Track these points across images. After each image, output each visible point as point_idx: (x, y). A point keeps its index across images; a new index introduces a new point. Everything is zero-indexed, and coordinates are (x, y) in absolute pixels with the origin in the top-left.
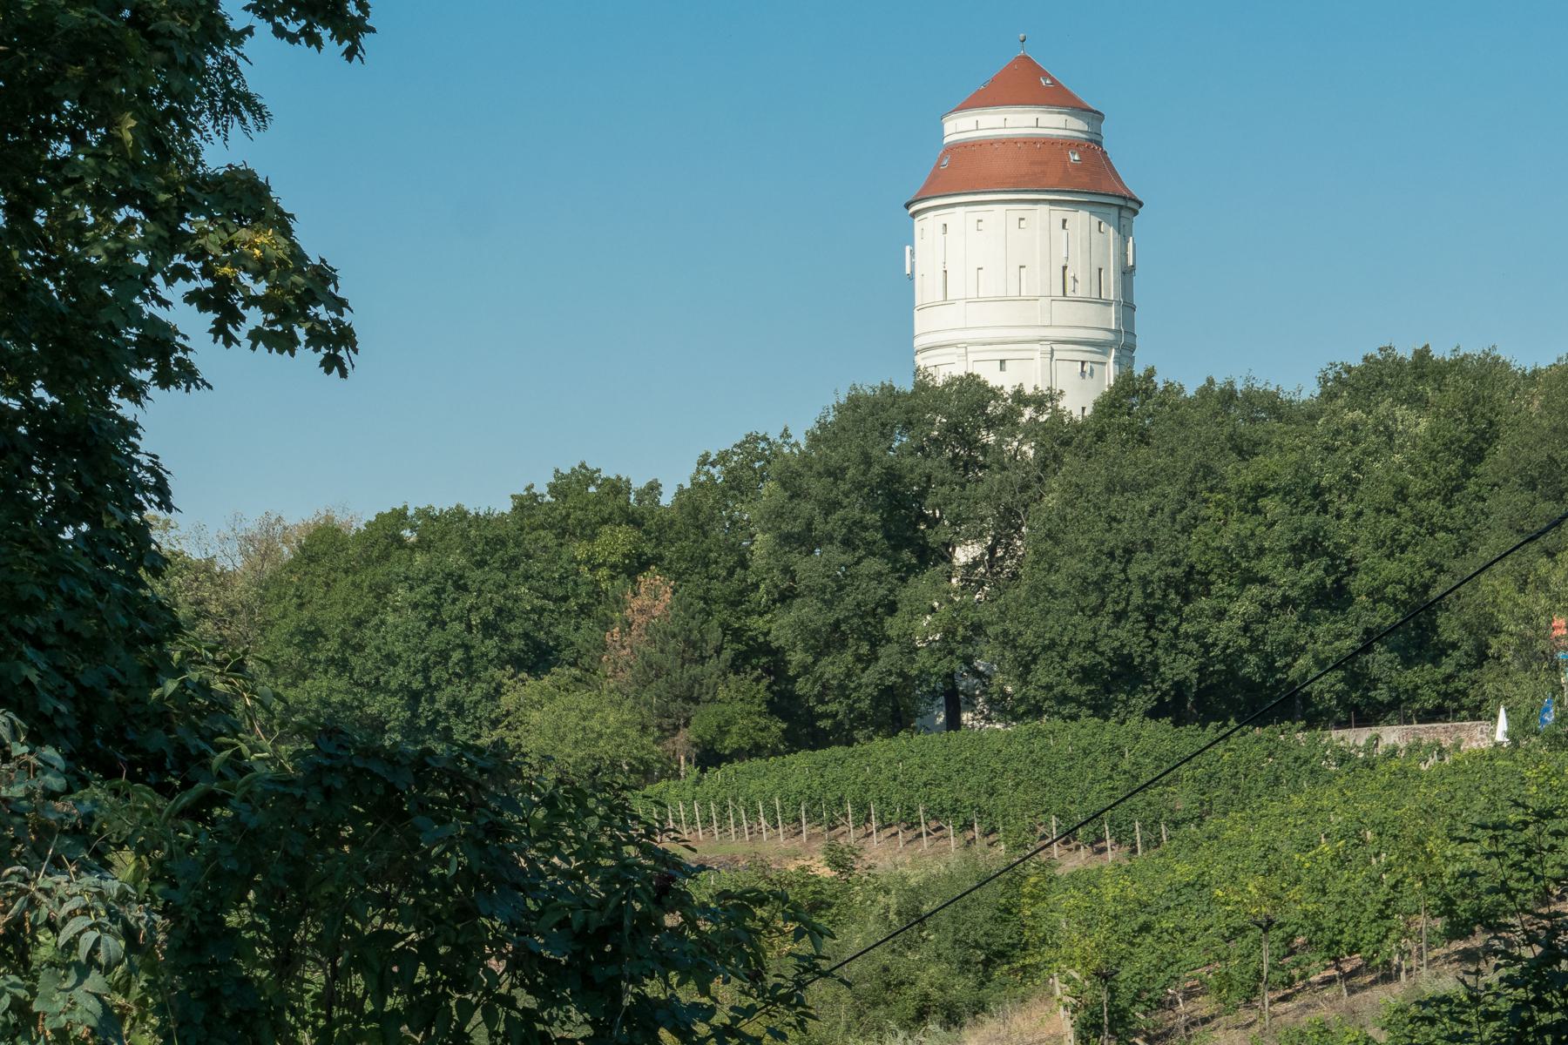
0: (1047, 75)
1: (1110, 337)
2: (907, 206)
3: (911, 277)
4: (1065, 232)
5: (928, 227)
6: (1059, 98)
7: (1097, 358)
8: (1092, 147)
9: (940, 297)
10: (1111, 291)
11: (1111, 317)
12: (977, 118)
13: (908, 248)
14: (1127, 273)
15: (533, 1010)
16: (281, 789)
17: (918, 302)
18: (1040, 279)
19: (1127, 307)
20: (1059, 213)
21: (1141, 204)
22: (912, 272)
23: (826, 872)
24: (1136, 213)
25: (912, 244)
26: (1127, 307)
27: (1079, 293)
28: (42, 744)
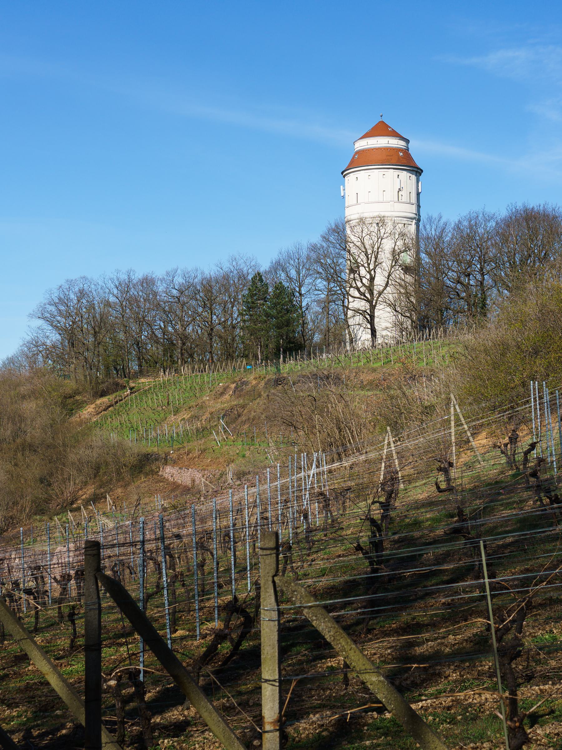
0: (390, 128)
1: (414, 216)
2: (342, 173)
3: (343, 197)
4: (398, 180)
5: (351, 179)
6: (395, 134)
7: (410, 223)
8: (406, 151)
9: (356, 202)
10: (414, 200)
11: (414, 209)
12: (368, 141)
13: (342, 187)
14: (418, 194)
15: (229, 641)
16: (79, 564)
17: (346, 205)
18: (392, 194)
19: (419, 206)
20: (397, 172)
21: (422, 171)
22: (344, 195)
23: (315, 369)
24: (420, 175)
25: (344, 186)
26: (419, 206)
27: (403, 200)
28: (216, 636)
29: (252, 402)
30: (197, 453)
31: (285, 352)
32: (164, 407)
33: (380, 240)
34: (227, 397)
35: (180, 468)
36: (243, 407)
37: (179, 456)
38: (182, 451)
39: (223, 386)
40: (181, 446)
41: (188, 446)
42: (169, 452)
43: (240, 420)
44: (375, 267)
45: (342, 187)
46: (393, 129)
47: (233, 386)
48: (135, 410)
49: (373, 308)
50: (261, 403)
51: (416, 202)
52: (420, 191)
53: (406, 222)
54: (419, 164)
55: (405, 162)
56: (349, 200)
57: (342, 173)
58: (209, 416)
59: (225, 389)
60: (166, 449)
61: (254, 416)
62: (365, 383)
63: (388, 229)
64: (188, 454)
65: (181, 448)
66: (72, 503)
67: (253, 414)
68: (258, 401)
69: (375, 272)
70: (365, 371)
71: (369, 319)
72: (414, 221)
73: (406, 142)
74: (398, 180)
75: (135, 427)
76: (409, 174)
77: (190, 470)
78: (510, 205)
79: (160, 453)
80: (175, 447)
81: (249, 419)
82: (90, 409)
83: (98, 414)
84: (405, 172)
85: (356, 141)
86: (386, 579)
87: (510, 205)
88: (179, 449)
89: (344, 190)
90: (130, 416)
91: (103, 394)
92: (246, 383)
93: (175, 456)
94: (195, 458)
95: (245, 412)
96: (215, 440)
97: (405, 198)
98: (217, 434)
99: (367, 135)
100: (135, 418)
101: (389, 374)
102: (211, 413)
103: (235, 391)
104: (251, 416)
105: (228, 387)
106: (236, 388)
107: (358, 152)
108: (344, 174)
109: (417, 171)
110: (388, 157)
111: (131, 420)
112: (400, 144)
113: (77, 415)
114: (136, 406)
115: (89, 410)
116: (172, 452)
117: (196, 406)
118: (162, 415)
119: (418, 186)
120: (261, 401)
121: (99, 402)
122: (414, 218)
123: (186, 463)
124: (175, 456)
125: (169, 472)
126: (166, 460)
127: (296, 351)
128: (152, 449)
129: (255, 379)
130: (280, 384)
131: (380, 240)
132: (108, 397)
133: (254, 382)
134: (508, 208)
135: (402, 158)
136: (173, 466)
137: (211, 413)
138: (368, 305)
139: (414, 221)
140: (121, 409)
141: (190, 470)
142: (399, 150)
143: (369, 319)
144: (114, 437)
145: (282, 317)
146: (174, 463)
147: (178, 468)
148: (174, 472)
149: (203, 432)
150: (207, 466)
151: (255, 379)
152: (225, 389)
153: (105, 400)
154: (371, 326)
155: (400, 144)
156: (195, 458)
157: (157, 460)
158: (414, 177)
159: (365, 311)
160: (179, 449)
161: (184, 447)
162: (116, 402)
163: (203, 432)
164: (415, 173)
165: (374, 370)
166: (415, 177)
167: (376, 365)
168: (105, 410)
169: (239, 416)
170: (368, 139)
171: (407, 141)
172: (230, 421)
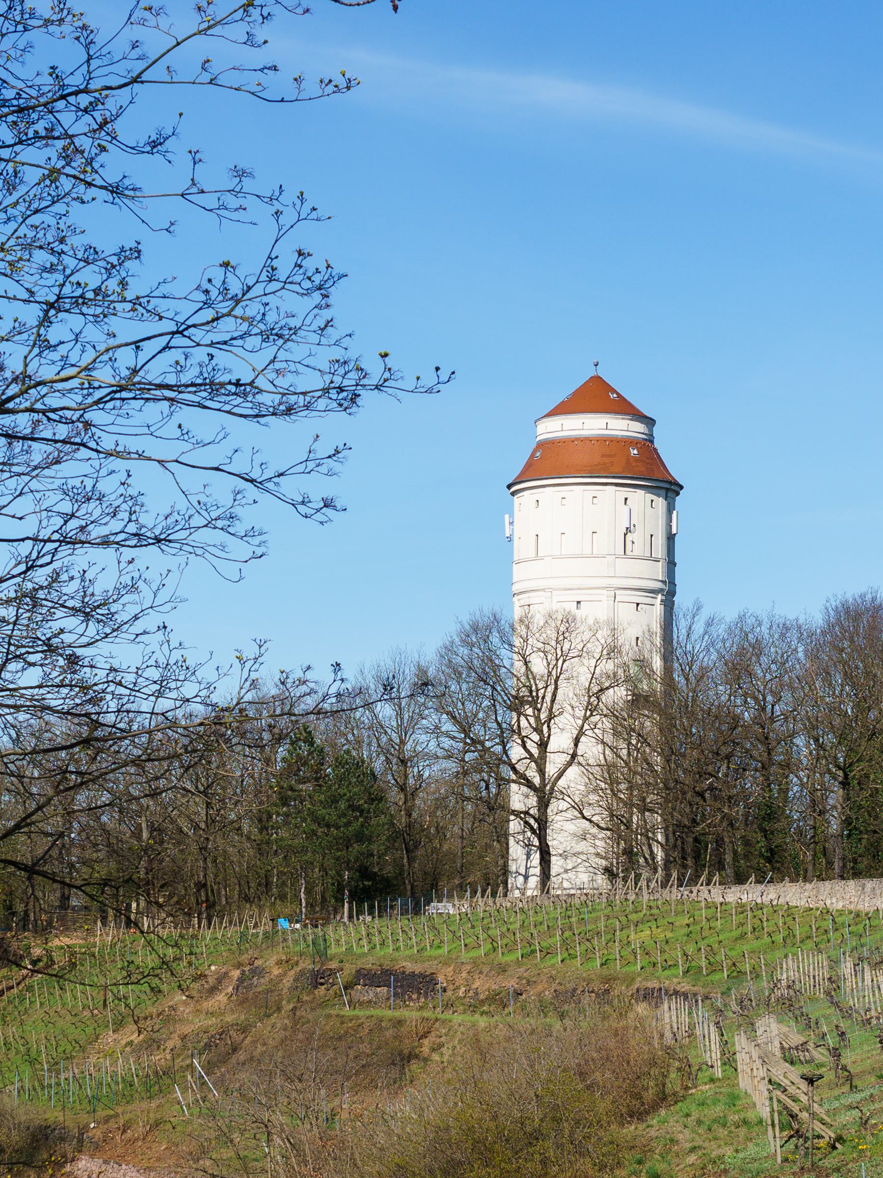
0: (614, 391)
1: (660, 585)
3: (510, 539)
4: (626, 508)
5: (525, 501)
6: (625, 408)
7: (649, 601)
8: (647, 445)
9: (532, 554)
10: (660, 551)
11: (659, 571)
13: (507, 517)
14: (671, 538)
19: (671, 564)
20: (624, 492)
21: (681, 487)
24: (678, 494)
25: (512, 515)
26: (671, 564)
27: (636, 553)
29: (261, 1020)
30: (139, 1130)
31: (352, 897)
32: (96, 1012)
33: (560, 662)
35: (106, 1162)
36: (244, 1029)
37: (105, 1134)
38: (112, 1125)
39: (216, 972)
40: (112, 1112)
42: (88, 1124)
43: (233, 1060)
45: (507, 517)
46: (619, 395)
47: (236, 973)
48: (38, 1013)
50: (279, 1025)
51: (665, 556)
52: (674, 531)
53: (638, 600)
54: (676, 472)
55: (643, 469)
56: (522, 548)
58: (179, 1043)
59: (222, 978)
60: (84, 1118)
61: (263, 1054)
62: (482, 997)
63: (578, 640)
64: (124, 1131)
65: (112, 1116)
67: (260, 1048)
68: (273, 1019)
69: (548, 726)
70: (485, 970)
71: (536, 826)
72: (660, 597)
73: (647, 424)
74: (626, 508)
75: (33, 1054)
76: (650, 496)
77: (124, 1166)
78: (832, 600)
81: (252, 1058)
84: (641, 492)
85: (539, 419)
87: (832, 600)
88: (107, 1120)
89: (511, 523)
92: (257, 972)
93: (98, 1134)
94: (137, 1139)
95: (246, 1042)
96: (179, 1103)
97: (639, 547)
98: (184, 1091)
100: (35, 1034)
101: (528, 982)
102: (183, 1038)
103: (238, 987)
104: (256, 1053)
105: (226, 974)
106: (241, 980)
107: (541, 445)
110: (606, 460)
111: (28, 1037)
114: (42, 1004)
116: (92, 1125)
117: (159, 1015)
118: (89, 1030)
120: (280, 1021)
122: (660, 591)
123: (119, 1150)
124: (98, 1134)
126: (80, 1141)
127: (371, 899)
128: (54, 1115)
129: (279, 963)
130: (322, 984)
131: (560, 662)
133: (276, 971)
134: (828, 604)
135: (636, 460)
136: (92, 1156)
137: (183, 1038)
139: (660, 597)
140: (10, 1008)
141: (124, 1166)
143: (536, 826)
145: (348, 824)
146: (97, 1148)
147: (101, 1161)
148: (94, 1168)
151: (279, 963)
152: (222, 978)
154: (540, 842)
156: (137, 1139)
157: (62, 1139)
158: (660, 503)
159: (527, 813)
161: (117, 1115)
164: (663, 492)
165: (503, 969)
166: (665, 502)
167: (510, 958)
169: (235, 1050)
170: (563, 417)
171: (650, 422)
172: (215, 1059)
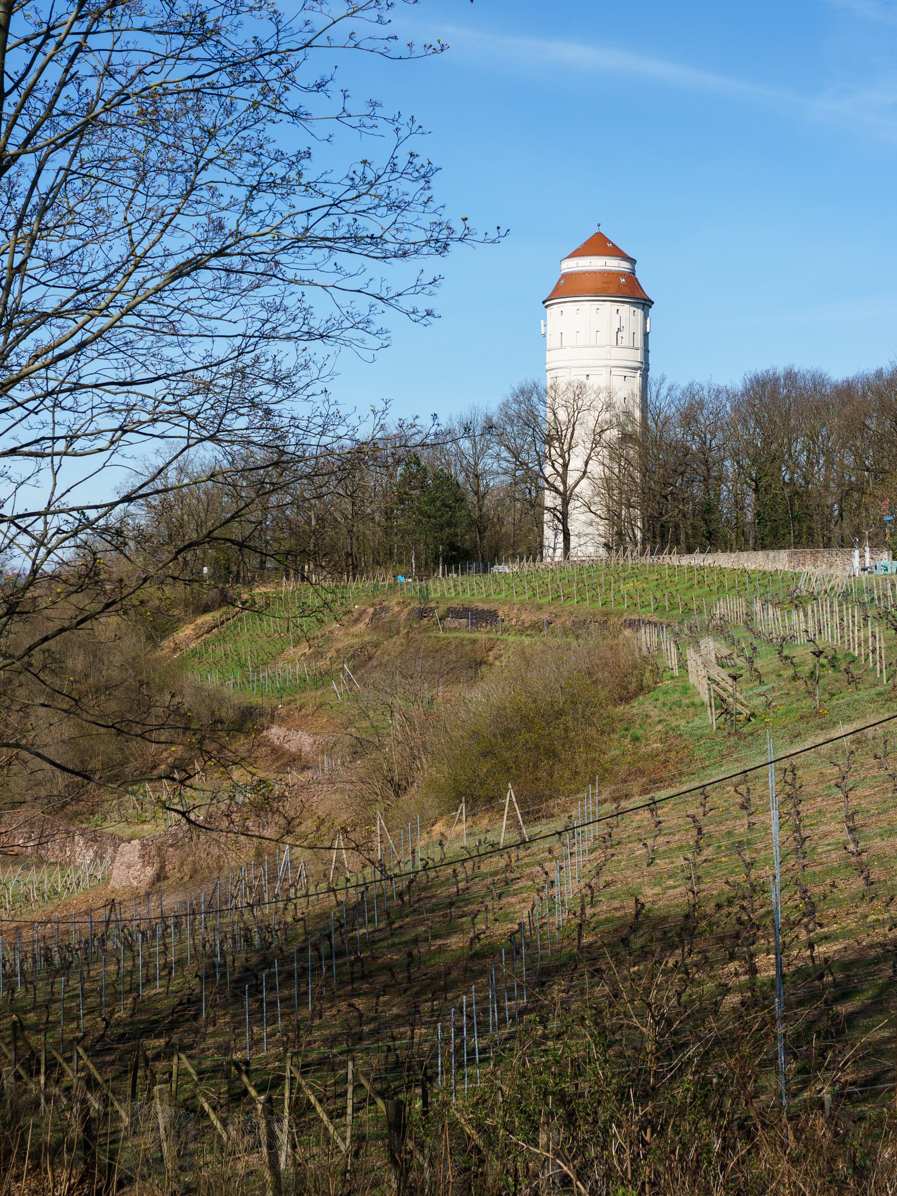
1: (639, 365)
2: (544, 302)
3: (544, 335)
5: (554, 311)
6: (617, 253)
8: (631, 276)
9: (558, 345)
10: (639, 343)
11: (638, 355)
14: (646, 335)
18: (607, 336)
19: (646, 351)
20: (617, 306)
25: (545, 321)
26: (646, 351)
30: (310, 709)
34: (362, 625)
35: (288, 729)
38: (293, 706)
41: (301, 698)
42: (277, 707)
43: (369, 665)
44: (570, 448)
47: (371, 610)
48: (246, 636)
49: (566, 503)
54: (650, 293)
57: (544, 302)
58: (335, 654)
59: (362, 613)
60: (275, 701)
61: (388, 661)
66: (154, 767)
68: (394, 639)
76: (633, 309)
79: (266, 705)
80: (286, 699)
82: (187, 631)
83: (198, 638)
86: (316, 953)
88: (289, 703)
90: (239, 645)
91: (206, 609)
92: (384, 609)
93: (284, 712)
97: (626, 341)
98: (338, 684)
99: (577, 254)
104: (384, 661)
106: (374, 614)
107: (565, 276)
108: (546, 303)
109: (645, 304)
112: (624, 266)
113: (171, 638)
115: (188, 632)
119: (645, 323)
120: (399, 640)
121: (200, 620)
122: (640, 368)
123: (297, 722)
124: (284, 712)
125: (275, 733)
126: (273, 716)
127: (456, 563)
128: (256, 700)
129: (398, 603)
132: (212, 614)
133: (396, 609)
136: (280, 726)
137: (338, 651)
138: (559, 501)
140: (228, 632)
142: (620, 274)
144: (213, 680)
146: (283, 721)
149: (322, 678)
150: (322, 728)
151: (398, 603)
153: (207, 618)
155: (624, 266)
157: (261, 715)
158: (639, 312)
159: (555, 509)
160: (289, 703)
161: (295, 700)
162: (222, 623)
163: (322, 678)
165: (540, 608)
168: (208, 632)
169: (370, 659)
171: (633, 261)
